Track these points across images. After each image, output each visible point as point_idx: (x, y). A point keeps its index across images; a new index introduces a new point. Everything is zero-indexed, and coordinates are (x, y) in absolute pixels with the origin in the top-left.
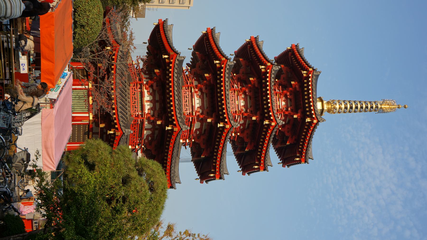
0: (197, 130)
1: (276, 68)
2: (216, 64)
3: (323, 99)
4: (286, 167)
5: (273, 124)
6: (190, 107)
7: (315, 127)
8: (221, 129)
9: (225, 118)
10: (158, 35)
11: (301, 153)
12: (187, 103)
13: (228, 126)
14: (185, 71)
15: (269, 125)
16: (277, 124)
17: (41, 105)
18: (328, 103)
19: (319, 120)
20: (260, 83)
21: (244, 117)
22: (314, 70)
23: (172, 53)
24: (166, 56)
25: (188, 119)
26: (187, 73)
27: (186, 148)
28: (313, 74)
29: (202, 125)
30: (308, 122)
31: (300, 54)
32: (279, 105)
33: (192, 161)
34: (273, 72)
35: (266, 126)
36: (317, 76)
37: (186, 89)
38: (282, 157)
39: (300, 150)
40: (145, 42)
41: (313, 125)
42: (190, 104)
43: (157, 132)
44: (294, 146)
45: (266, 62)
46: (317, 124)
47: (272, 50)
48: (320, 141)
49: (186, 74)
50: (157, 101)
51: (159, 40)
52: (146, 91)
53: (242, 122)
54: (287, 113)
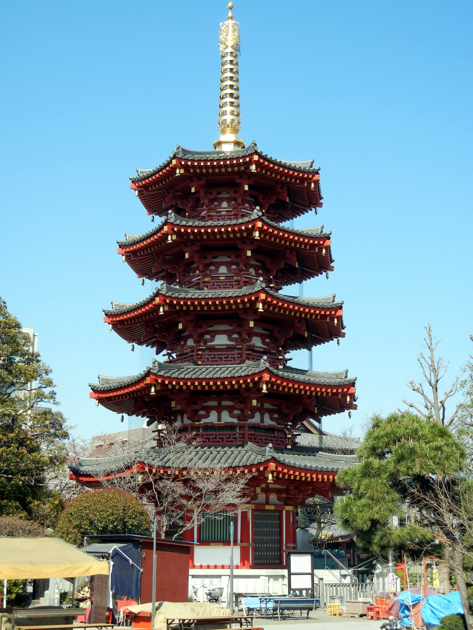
0: (264, 343)
1: (172, 216)
2: (164, 311)
3: (216, 142)
4: (321, 201)
5: (259, 224)
6: (229, 353)
7: (265, 158)
8: (266, 307)
9: (250, 300)
10: (115, 400)
11: (303, 180)
12: (223, 357)
13: (263, 296)
14: (171, 358)
15: (261, 230)
16: (260, 219)
17: (331, 595)
18: (223, 132)
19: (254, 151)
20: (193, 243)
21: (244, 268)
22: (174, 157)
23: (148, 380)
24: (153, 389)
25: (248, 356)
26: (174, 355)
27: (291, 359)
28: (181, 158)
29: (257, 335)
30: (256, 169)
31: (148, 177)
32: (227, 211)
33: (310, 350)
34: (178, 222)
35: (262, 236)
36: (184, 151)
37: (201, 358)
38: (305, 208)
39: (298, 182)
40: (120, 418)
41: (262, 161)
42: (224, 353)
43: (267, 406)
44: (293, 190)
45: (162, 232)
46: (260, 156)
47: (142, 223)
48: (288, 152)
49: (175, 357)
50: (219, 403)
51: (116, 398)
52: (203, 421)
53: (252, 271)
54: (240, 200)
